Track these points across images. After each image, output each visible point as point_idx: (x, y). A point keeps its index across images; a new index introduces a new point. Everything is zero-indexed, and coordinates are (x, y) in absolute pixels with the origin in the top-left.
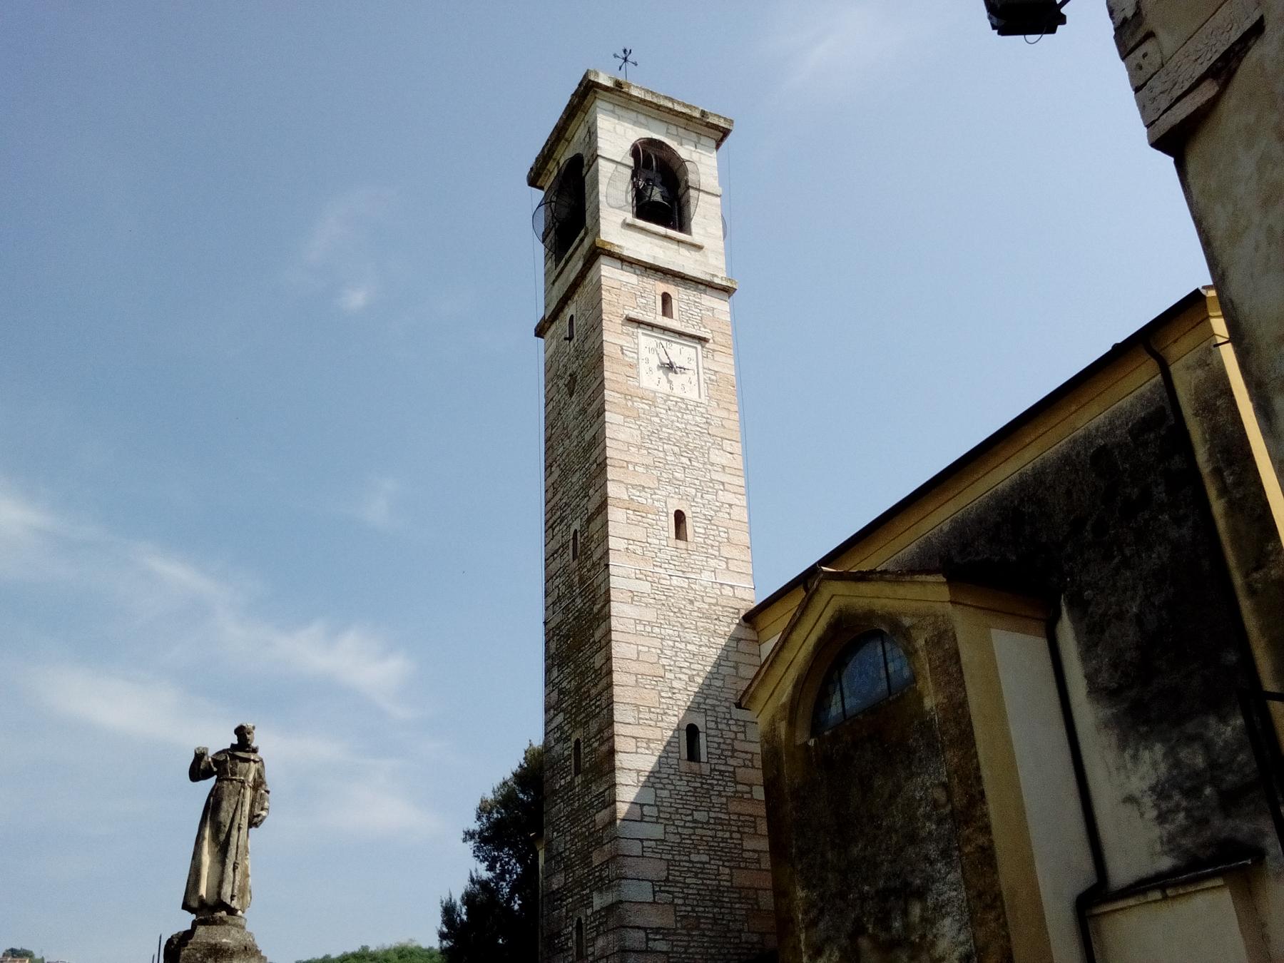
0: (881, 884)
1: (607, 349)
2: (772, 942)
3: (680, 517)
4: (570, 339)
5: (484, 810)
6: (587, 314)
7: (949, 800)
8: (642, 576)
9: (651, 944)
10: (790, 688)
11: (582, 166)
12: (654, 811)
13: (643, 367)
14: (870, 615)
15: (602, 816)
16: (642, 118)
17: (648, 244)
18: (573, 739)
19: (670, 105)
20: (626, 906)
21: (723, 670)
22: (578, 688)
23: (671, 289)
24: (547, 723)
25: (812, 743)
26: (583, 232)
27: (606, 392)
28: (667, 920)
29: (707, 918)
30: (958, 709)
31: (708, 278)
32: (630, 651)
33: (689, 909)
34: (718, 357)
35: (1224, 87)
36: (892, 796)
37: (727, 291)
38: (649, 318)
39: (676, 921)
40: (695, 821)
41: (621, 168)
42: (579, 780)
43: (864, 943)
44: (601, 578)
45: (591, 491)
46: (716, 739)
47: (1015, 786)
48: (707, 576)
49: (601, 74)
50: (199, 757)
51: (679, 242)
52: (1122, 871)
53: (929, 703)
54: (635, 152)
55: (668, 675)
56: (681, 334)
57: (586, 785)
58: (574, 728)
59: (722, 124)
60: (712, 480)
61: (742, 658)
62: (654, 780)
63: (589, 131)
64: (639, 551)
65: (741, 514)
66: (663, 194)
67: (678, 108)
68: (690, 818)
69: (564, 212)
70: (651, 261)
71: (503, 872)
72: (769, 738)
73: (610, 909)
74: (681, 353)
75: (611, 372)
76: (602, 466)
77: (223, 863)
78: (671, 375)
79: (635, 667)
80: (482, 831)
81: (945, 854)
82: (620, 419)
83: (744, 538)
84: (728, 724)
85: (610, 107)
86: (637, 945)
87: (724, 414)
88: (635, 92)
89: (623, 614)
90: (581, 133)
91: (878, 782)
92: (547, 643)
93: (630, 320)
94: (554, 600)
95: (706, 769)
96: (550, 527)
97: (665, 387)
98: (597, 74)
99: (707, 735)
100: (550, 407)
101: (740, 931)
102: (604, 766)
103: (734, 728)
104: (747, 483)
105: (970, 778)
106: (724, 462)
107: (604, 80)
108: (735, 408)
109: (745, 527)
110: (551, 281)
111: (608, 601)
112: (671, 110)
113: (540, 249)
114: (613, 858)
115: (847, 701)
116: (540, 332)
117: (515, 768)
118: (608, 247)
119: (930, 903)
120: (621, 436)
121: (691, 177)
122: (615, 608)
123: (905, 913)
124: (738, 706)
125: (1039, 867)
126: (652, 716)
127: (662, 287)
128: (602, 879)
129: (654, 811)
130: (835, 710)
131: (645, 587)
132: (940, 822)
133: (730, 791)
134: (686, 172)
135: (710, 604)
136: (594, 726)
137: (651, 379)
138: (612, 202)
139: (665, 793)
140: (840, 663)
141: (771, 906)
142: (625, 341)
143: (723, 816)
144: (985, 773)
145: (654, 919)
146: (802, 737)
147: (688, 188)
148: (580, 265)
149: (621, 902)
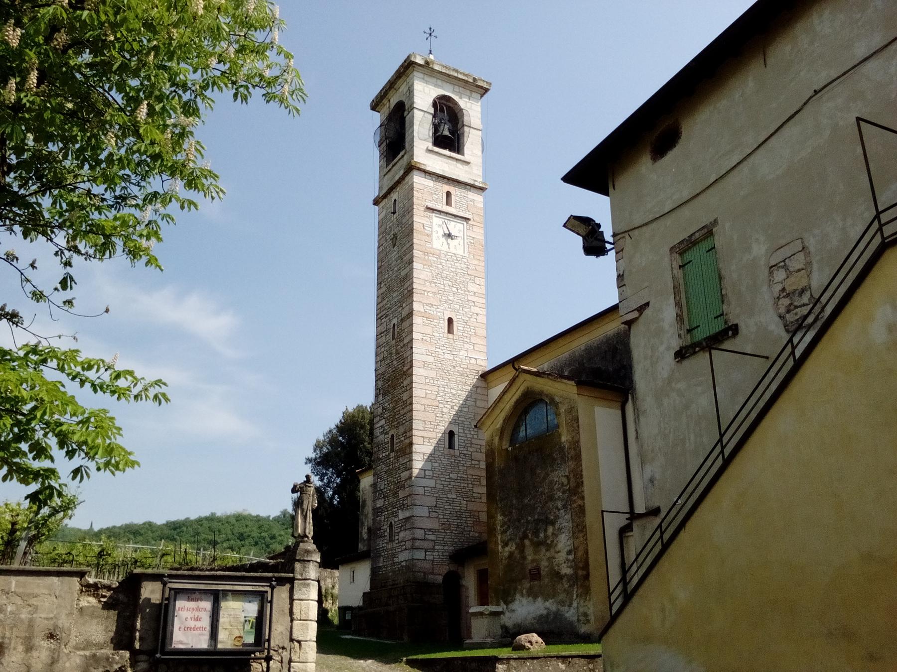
0: (536, 517)
1: (416, 226)
2: (485, 536)
3: (450, 321)
4: (394, 213)
5: (318, 446)
7: (569, 483)
8: (430, 353)
10: (501, 422)
11: (404, 110)
12: (430, 473)
13: (434, 236)
14: (541, 393)
15: (404, 475)
16: (439, 82)
19: (456, 75)
21: (468, 403)
22: (393, 409)
23: (451, 189)
25: (510, 449)
26: (402, 153)
27: (414, 251)
28: (436, 526)
30: (576, 444)
31: (472, 182)
34: (475, 229)
35: (641, 315)
36: (545, 478)
37: (482, 189)
38: (439, 207)
41: (426, 115)
42: (393, 455)
43: (527, 542)
44: (408, 353)
47: (598, 480)
48: (463, 353)
49: (418, 57)
50: (295, 486)
51: (457, 160)
53: (564, 439)
54: (435, 105)
55: (441, 405)
56: (456, 216)
57: (397, 457)
58: (391, 428)
59: (485, 86)
60: (468, 300)
61: (480, 397)
62: (431, 458)
63: (409, 89)
64: (429, 340)
65: (482, 319)
66: (450, 134)
67: (460, 76)
69: (391, 134)
70: (441, 173)
71: (329, 482)
72: (490, 444)
73: (408, 519)
74: (456, 227)
75: (417, 239)
76: (411, 292)
77: (305, 522)
78: (450, 240)
79: (424, 401)
80: (316, 459)
81: (565, 507)
83: (482, 332)
85: (421, 75)
86: (420, 537)
87: (476, 262)
88: (436, 67)
89: (419, 374)
90: (403, 88)
91: (538, 471)
92: (376, 381)
93: (428, 208)
96: (379, 318)
97: (445, 248)
98: (415, 57)
100: (381, 249)
102: (407, 450)
104: (487, 301)
105: (578, 475)
106: (475, 290)
107: (419, 60)
108: (482, 259)
109: (484, 326)
110: (382, 176)
111: (411, 366)
112: (456, 78)
113: (377, 153)
114: (410, 495)
116: (376, 202)
117: (337, 421)
118: (418, 165)
119: (556, 527)
120: (421, 276)
121: (466, 118)
122: (415, 370)
123: (546, 530)
127: (447, 188)
128: (403, 505)
129: (430, 473)
130: (522, 434)
131: (431, 359)
132: (564, 492)
133: (468, 463)
134: (463, 115)
137: (438, 243)
138: (422, 137)
139: (437, 465)
140: (526, 412)
141: (486, 520)
142: (424, 221)
144: (584, 473)
145: (428, 524)
146: (506, 445)
147: (463, 125)
148: (402, 172)
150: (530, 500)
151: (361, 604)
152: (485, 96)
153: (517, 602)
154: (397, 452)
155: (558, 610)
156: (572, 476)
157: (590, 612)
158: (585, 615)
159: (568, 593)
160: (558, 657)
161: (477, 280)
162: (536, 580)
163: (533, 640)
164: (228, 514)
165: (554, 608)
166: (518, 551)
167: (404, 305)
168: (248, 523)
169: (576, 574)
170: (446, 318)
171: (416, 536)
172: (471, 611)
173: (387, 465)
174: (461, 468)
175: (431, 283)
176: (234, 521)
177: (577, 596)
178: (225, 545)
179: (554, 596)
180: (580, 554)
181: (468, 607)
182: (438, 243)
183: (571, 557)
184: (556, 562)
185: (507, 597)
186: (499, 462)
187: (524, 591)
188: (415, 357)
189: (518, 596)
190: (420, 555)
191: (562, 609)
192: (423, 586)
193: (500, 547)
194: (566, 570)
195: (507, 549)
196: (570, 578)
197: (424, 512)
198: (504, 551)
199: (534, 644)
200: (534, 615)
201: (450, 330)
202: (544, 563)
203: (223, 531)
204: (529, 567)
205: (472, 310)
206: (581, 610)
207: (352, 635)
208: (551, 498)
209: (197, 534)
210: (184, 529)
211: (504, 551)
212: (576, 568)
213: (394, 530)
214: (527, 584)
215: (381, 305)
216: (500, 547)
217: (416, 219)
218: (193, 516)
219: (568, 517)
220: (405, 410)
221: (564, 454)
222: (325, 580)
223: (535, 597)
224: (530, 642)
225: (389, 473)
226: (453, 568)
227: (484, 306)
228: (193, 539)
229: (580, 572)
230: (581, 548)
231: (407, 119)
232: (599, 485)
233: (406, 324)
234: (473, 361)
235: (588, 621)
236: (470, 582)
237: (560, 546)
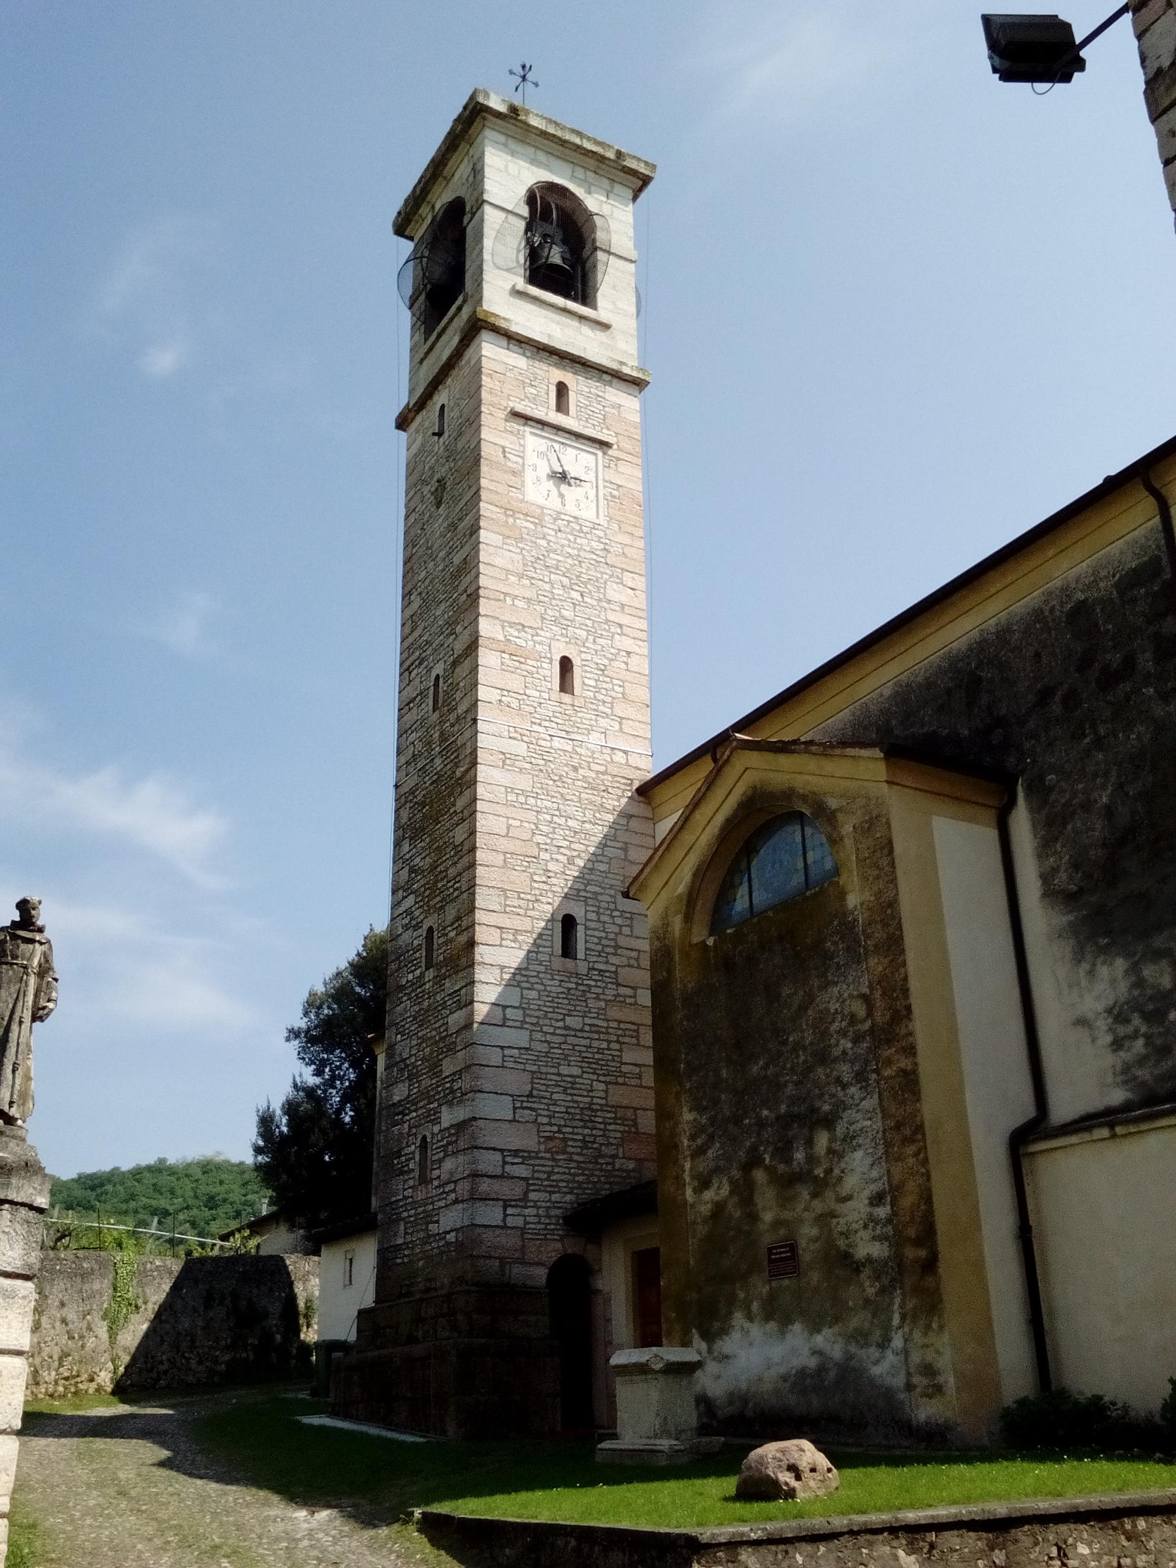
0: (783, 1108)
2: (650, 1171)
3: (566, 665)
4: (439, 434)
5: (313, 1004)
7: (870, 1014)
8: (517, 735)
13: (529, 476)
14: (789, 794)
15: (456, 1019)
16: (541, 156)
17: (543, 318)
19: (577, 141)
21: (610, 852)
22: (433, 867)
23: (569, 378)
25: (710, 942)
30: (887, 911)
32: (499, 825)
33: (555, 1129)
34: (622, 467)
36: (803, 1009)
37: (637, 384)
38: (539, 414)
39: (539, 1143)
40: (566, 1028)
41: (511, 218)
42: (430, 974)
43: (759, 1175)
44: (467, 735)
45: (459, 629)
46: (596, 933)
48: (595, 738)
49: (492, 95)
51: (582, 318)
53: (852, 900)
54: (531, 199)
56: (578, 436)
57: (439, 980)
58: (427, 914)
59: (642, 169)
60: (607, 621)
61: (635, 840)
62: (520, 978)
64: (515, 704)
65: (640, 664)
66: (564, 258)
68: (561, 1024)
69: (438, 271)
71: (334, 1078)
72: (660, 936)
73: (461, 1126)
74: (577, 460)
75: (487, 480)
76: (474, 597)
78: (564, 488)
79: (503, 844)
81: (860, 1077)
83: (643, 694)
85: (502, 138)
86: (491, 1170)
87: (627, 540)
88: (534, 122)
89: (492, 781)
90: (463, 171)
91: (786, 991)
92: (397, 811)
93: (516, 415)
94: (409, 757)
95: (583, 968)
96: (406, 670)
97: (554, 503)
98: (487, 95)
99: (587, 928)
101: (614, 1156)
103: (619, 921)
104: (651, 625)
105: (894, 996)
106: (624, 600)
107: (496, 103)
108: (640, 532)
109: (644, 680)
110: (419, 359)
111: (474, 763)
112: (578, 148)
114: (468, 1068)
116: (402, 423)
117: (352, 956)
118: (492, 320)
119: (840, 1130)
120: (499, 561)
121: (600, 236)
122: (483, 773)
123: (810, 1143)
127: (558, 374)
128: (453, 1091)
130: (741, 904)
132: (856, 1040)
133: (610, 993)
134: (593, 228)
135: (598, 772)
137: (538, 490)
139: (533, 994)
140: (749, 849)
142: (507, 441)
144: (914, 984)
146: (700, 934)
147: (596, 249)
148: (456, 339)
150: (766, 1067)
151: (353, 1337)
152: (643, 196)
153: (736, 1335)
154: (439, 966)
155: (850, 1357)
156: (878, 994)
157: (945, 1361)
158: (929, 1370)
159: (878, 1308)
160: (894, 1530)
161: (628, 579)
162: (787, 1276)
163: (804, 1465)
164: (189, 1159)
165: (836, 1352)
166: (735, 1199)
167: (459, 629)
168: (224, 1177)
169: (898, 1257)
170: (557, 658)
171: (482, 1167)
172: (616, 1360)
173: (418, 1000)
174: (591, 1003)
175: (521, 577)
176: (198, 1173)
177: (903, 1317)
178: (181, 1217)
179: (837, 1319)
180: (907, 1201)
181: (611, 1346)
182: (538, 490)
183: (883, 1212)
184: (840, 1225)
185: (709, 1321)
186: (684, 977)
187: (755, 1306)
188: (483, 741)
189: (738, 1318)
190: (491, 1215)
191: (862, 1353)
192: (497, 1294)
193: (689, 1192)
194: (868, 1248)
195: (708, 1195)
196: (877, 1267)
197: (501, 1108)
198: (700, 1199)
199: (807, 1474)
200: (782, 1370)
201: (566, 683)
202: (808, 1232)
203: (179, 1192)
204: (767, 1239)
205: (618, 644)
206: (915, 1358)
207: (334, 1414)
208: (823, 1057)
209: (133, 1197)
210: (109, 1188)
211: (700, 1201)
212: (897, 1241)
213: (434, 1155)
214: (761, 1287)
215: (410, 640)
216: (689, 1192)
217: (485, 434)
218: (126, 1166)
219: (871, 1103)
220: (460, 866)
221: (857, 941)
222: (305, 1281)
223: (785, 1322)
224: (793, 1469)
225: (422, 1019)
226: (573, 1246)
227: (644, 636)
228: (124, 1207)
229: (910, 1253)
230: (911, 1185)
231: (469, 230)
232: (952, 1015)
233: (462, 670)
234: (619, 757)
235: (938, 1389)
236: (615, 1282)
237: (851, 1183)
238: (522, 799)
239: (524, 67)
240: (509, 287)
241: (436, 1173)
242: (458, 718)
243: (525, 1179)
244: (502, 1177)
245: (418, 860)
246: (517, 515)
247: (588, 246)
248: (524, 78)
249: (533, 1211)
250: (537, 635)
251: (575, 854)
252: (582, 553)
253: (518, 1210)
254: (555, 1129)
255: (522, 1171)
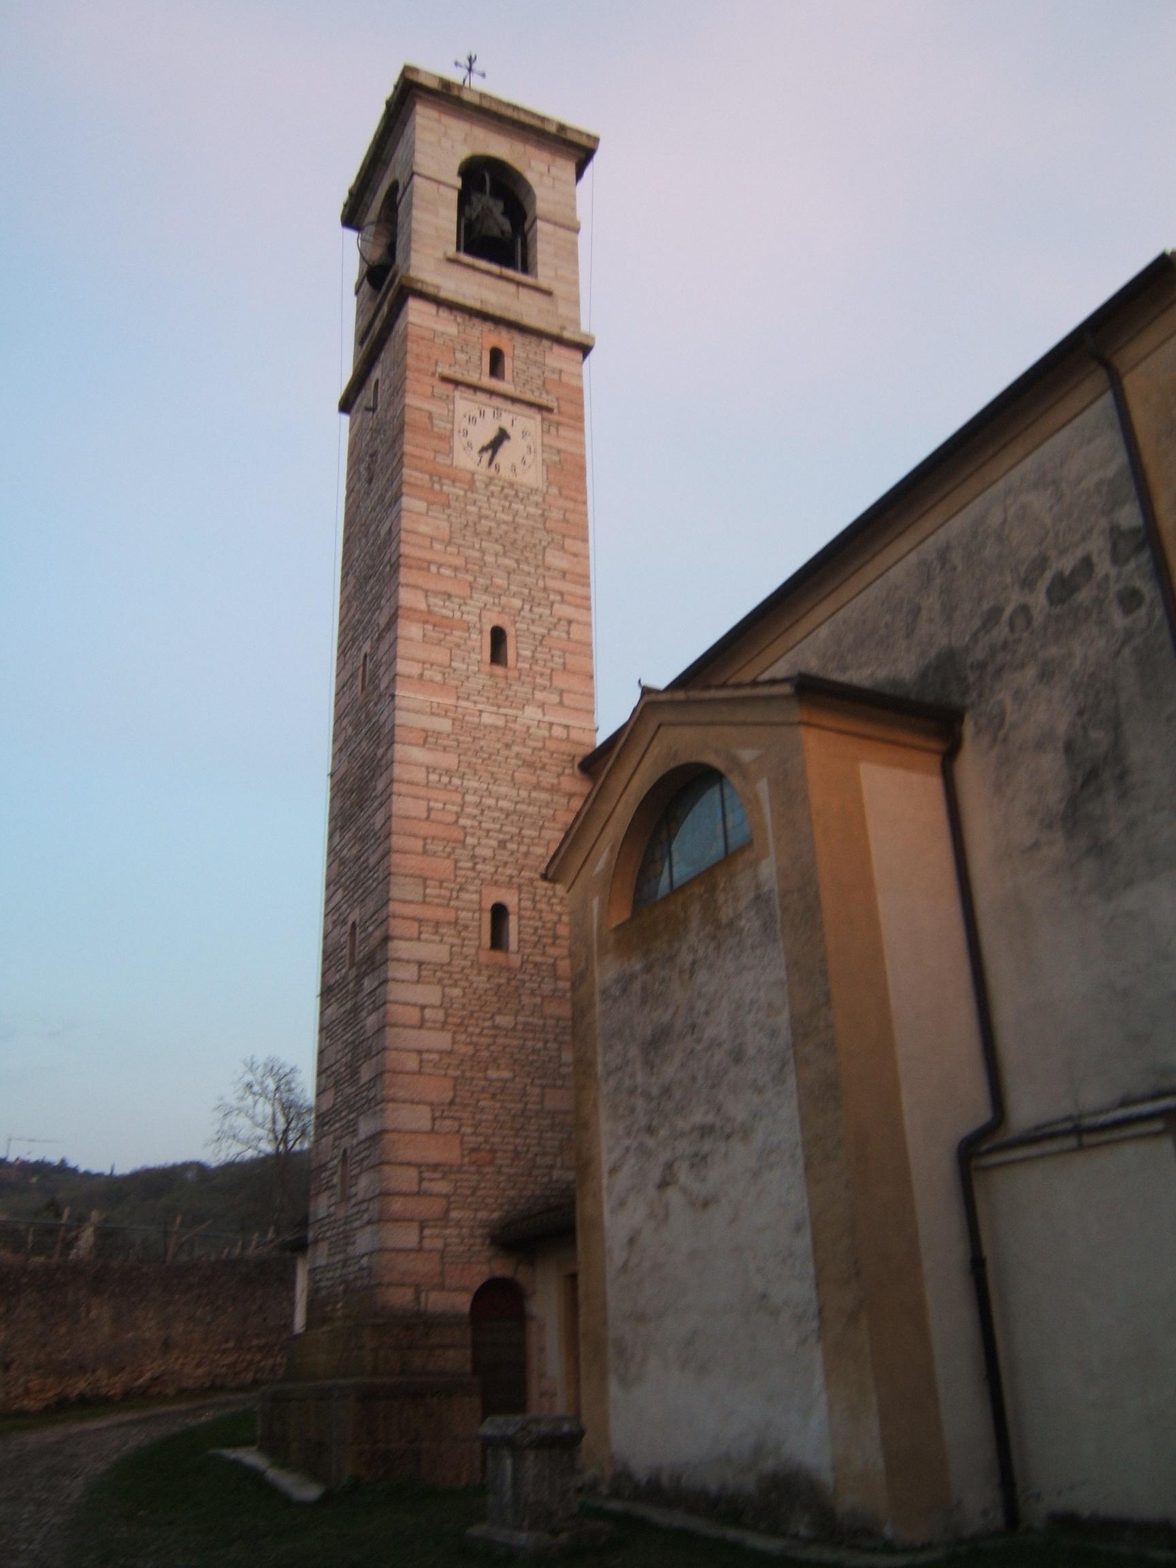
1: (410, 416)
3: (498, 636)
6: (391, 374)
9: (425, 1185)
13: (458, 442)
17: (478, 286)
18: (350, 923)
20: (394, 1136)
23: (502, 339)
24: (328, 901)
28: (451, 1154)
29: (505, 1151)
32: (416, 808)
33: (481, 1139)
38: (473, 378)
39: (463, 1156)
40: (495, 1027)
42: (353, 973)
45: (383, 602)
46: (531, 923)
51: (519, 284)
52: (1026, 1111)
56: (514, 400)
68: (488, 1023)
79: (424, 829)
82: (420, 506)
84: (549, 903)
86: (405, 1187)
93: (445, 379)
94: (343, 744)
95: (515, 960)
99: (520, 918)
101: (552, 1167)
103: (558, 908)
115: (675, 870)
118: (419, 286)
120: (422, 528)
124: (544, 877)
125: (906, 1101)
126: (443, 892)
133: (547, 988)
134: (533, 201)
135: (534, 749)
136: (371, 905)
139: (456, 992)
143: (535, 1021)
145: (433, 1152)
149: (384, 1131)
170: (488, 629)
171: (393, 1185)
197: (418, 1118)
226: (502, 1268)
238: (445, 779)
239: (470, 60)
240: (440, 255)
241: (353, 1190)
242: (380, 696)
243: (447, 1196)
244: (418, 1194)
245: (345, 851)
246: (445, 481)
247: (530, 218)
248: (470, 70)
249: (455, 1232)
250: (465, 604)
251: (508, 837)
252: (519, 520)
253: (437, 1231)
254: (481, 1139)
255: (442, 1187)
